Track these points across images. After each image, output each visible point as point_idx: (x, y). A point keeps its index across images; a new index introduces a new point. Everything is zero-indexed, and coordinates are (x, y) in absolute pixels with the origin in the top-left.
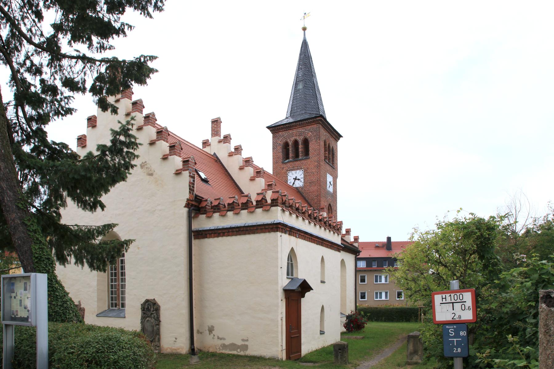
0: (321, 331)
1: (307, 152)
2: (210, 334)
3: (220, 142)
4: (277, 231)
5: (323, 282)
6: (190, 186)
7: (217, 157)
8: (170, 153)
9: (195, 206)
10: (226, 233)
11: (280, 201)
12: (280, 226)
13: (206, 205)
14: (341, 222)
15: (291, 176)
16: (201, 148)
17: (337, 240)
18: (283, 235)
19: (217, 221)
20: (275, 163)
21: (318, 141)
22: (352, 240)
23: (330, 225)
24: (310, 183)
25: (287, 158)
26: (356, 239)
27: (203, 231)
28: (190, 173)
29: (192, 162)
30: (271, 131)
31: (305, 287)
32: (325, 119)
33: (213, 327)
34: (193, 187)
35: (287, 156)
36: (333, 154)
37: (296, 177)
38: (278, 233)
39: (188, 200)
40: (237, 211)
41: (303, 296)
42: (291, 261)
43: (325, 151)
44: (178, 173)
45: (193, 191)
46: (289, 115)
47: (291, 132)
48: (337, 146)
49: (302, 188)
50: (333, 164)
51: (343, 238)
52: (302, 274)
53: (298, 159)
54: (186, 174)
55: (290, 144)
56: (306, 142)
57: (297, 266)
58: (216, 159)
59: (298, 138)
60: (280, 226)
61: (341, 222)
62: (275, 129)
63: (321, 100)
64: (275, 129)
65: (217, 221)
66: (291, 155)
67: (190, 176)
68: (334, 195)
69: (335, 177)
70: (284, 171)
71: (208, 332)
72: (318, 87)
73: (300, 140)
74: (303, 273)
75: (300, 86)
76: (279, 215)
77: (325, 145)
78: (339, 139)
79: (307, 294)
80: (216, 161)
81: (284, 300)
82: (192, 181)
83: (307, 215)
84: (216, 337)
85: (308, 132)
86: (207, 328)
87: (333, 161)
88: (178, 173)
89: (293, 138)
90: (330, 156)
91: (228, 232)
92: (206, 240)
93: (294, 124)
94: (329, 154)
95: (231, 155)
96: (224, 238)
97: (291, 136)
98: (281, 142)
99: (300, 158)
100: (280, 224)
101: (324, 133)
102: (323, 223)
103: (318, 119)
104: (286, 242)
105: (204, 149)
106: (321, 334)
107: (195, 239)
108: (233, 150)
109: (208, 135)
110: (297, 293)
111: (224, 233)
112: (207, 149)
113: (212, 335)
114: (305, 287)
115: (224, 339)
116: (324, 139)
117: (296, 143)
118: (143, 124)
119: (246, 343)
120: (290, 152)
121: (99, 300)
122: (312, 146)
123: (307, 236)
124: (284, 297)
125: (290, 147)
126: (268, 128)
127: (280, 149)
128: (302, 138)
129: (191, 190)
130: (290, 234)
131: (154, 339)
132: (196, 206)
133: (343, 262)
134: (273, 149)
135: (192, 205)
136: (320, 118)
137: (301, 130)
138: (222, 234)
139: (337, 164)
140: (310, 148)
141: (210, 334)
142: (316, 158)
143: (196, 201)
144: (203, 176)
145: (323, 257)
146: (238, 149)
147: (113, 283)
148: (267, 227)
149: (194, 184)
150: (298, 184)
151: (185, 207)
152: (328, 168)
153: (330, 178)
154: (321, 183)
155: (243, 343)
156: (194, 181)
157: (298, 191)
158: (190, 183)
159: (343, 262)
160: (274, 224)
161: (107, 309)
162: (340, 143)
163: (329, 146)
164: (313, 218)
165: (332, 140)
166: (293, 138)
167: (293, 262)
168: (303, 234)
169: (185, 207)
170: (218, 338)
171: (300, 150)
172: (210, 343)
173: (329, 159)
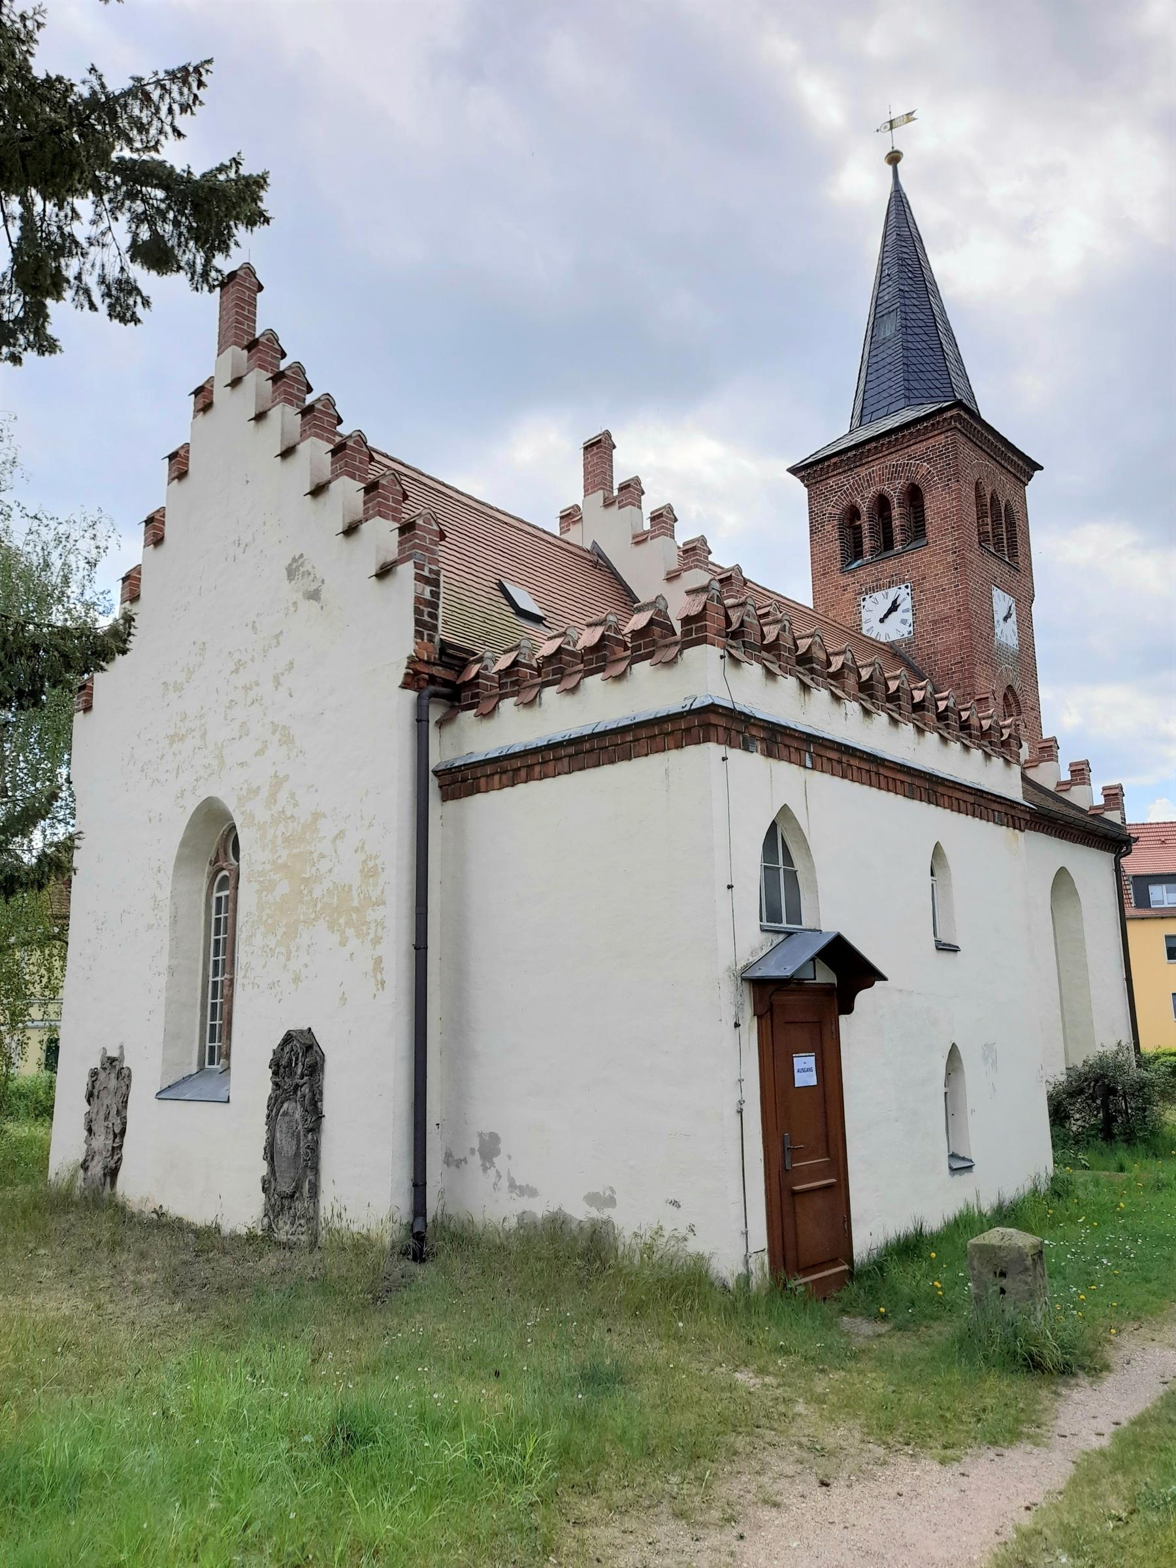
0: (953, 1156)
1: (917, 529)
2: (485, 1169)
3: (608, 503)
4: (707, 740)
5: (946, 948)
6: (418, 611)
7: (601, 555)
8: (366, 511)
9: (446, 683)
10: (537, 769)
11: (714, 623)
12: (714, 719)
13: (478, 675)
14: (1054, 740)
15: (874, 606)
16: (557, 534)
17: (1000, 779)
18: (736, 754)
19: (512, 728)
20: (819, 575)
21: (954, 486)
22: (1099, 800)
23: (965, 726)
24: (935, 622)
25: (858, 555)
26: (1114, 796)
27: (468, 766)
28: (417, 566)
29: (430, 532)
30: (802, 479)
31: (848, 970)
32: (975, 416)
33: (495, 1138)
34: (434, 616)
35: (853, 550)
36: (1011, 525)
37: (886, 616)
38: (712, 745)
39: (412, 661)
40: (570, 683)
41: (848, 1009)
42: (788, 860)
43: (981, 516)
44: (384, 572)
45: (434, 628)
46: (856, 423)
47: (863, 472)
48: (1024, 498)
49: (909, 643)
50: (1013, 556)
51: (1031, 774)
52: (830, 912)
53: (891, 553)
54: (407, 570)
55: (864, 508)
56: (914, 496)
57: (814, 883)
58: (599, 563)
59: (886, 488)
60: (714, 719)
61: (1054, 740)
62: (811, 471)
63: (959, 360)
64: (811, 471)
65: (512, 728)
66: (867, 544)
67: (419, 578)
68: (1026, 657)
69: (1024, 598)
70: (849, 595)
71: (476, 1160)
72: (946, 322)
73: (894, 490)
74: (835, 908)
75: (890, 328)
76: (707, 676)
77: (979, 496)
78: (1030, 478)
79: (863, 998)
80: (596, 565)
81: (750, 1026)
82: (427, 595)
83: (851, 681)
84: (504, 1183)
85: (918, 462)
86: (476, 1144)
87: (1013, 545)
88: (384, 572)
89: (873, 489)
90: (1003, 535)
91: (545, 762)
92: (479, 801)
93: (874, 444)
94: (996, 522)
95: (640, 540)
96: (533, 784)
97: (864, 486)
98: (834, 508)
99: (898, 548)
100: (712, 708)
101: (974, 462)
102: (930, 715)
103: (948, 414)
104: (757, 785)
105: (564, 537)
106: (953, 1170)
107: (446, 797)
108: (647, 526)
109: (573, 492)
110: (807, 997)
111: (530, 767)
112: (575, 535)
113: (492, 1172)
114: (848, 970)
115: (531, 1192)
116: (973, 478)
117: (882, 504)
118: (297, 437)
119: (607, 1213)
120: (866, 532)
121: (171, 1037)
122: (935, 504)
123: (855, 762)
124: (748, 1010)
125: (864, 517)
126: (794, 471)
127: (831, 530)
128: (900, 483)
129: (424, 624)
130: (769, 754)
131: (298, 1188)
132: (445, 681)
133: (1062, 878)
134: (812, 532)
135: (432, 679)
136: (954, 412)
137: (894, 460)
138: (523, 773)
139: (1028, 556)
140: (928, 514)
141: (485, 1169)
142: (949, 542)
143: (446, 666)
144: (526, 601)
145: (937, 846)
146: (664, 519)
147: (219, 979)
148: (669, 727)
149: (435, 606)
150: (896, 630)
151: (405, 685)
152: (995, 567)
153: (1001, 602)
154: (977, 622)
155: (594, 1213)
156: (435, 594)
157: (894, 652)
158: (418, 600)
159: (1062, 878)
160: (691, 712)
161: (194, 1069)
162: (1035, 488)
163: (994, 499)
164: (880, 694)
165: (1001, 484)
166: (873, 489)
167: (798, 865)
168: (834, 755)
169: (405, 685)
170: (512, 1186)
171: (896, 523)
172: (490, 1202)
173: (998, 544)
